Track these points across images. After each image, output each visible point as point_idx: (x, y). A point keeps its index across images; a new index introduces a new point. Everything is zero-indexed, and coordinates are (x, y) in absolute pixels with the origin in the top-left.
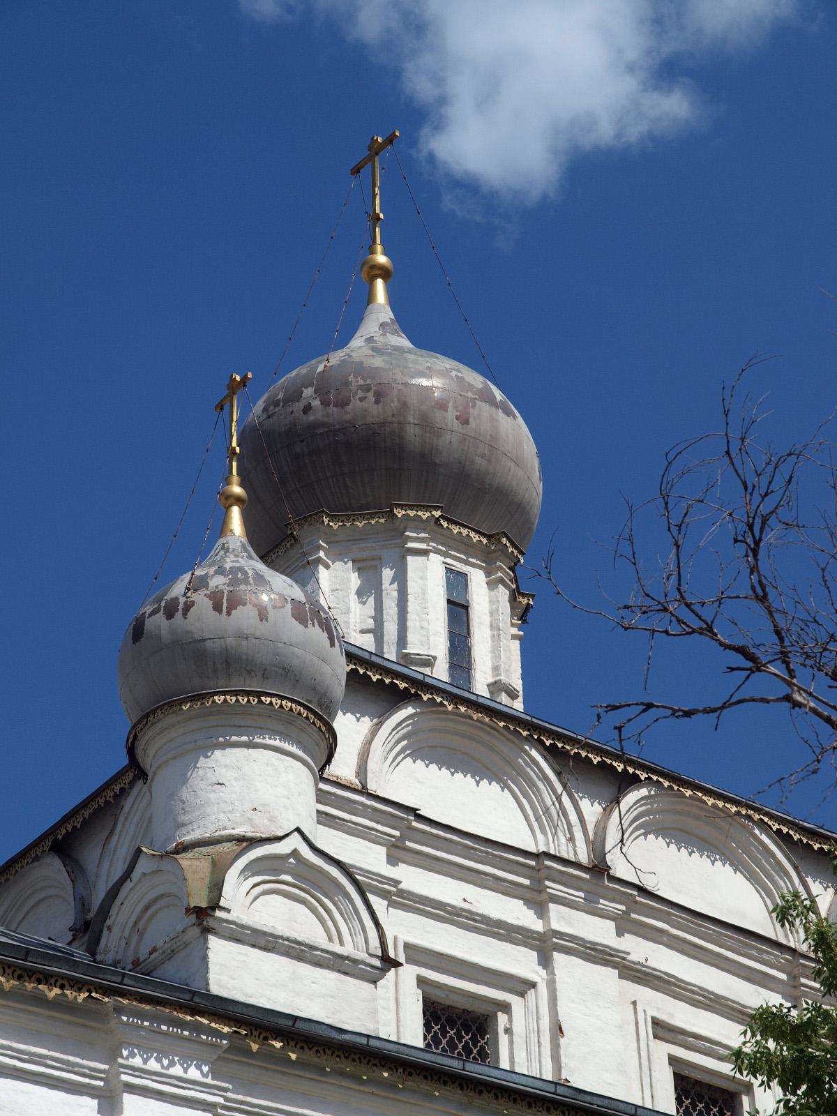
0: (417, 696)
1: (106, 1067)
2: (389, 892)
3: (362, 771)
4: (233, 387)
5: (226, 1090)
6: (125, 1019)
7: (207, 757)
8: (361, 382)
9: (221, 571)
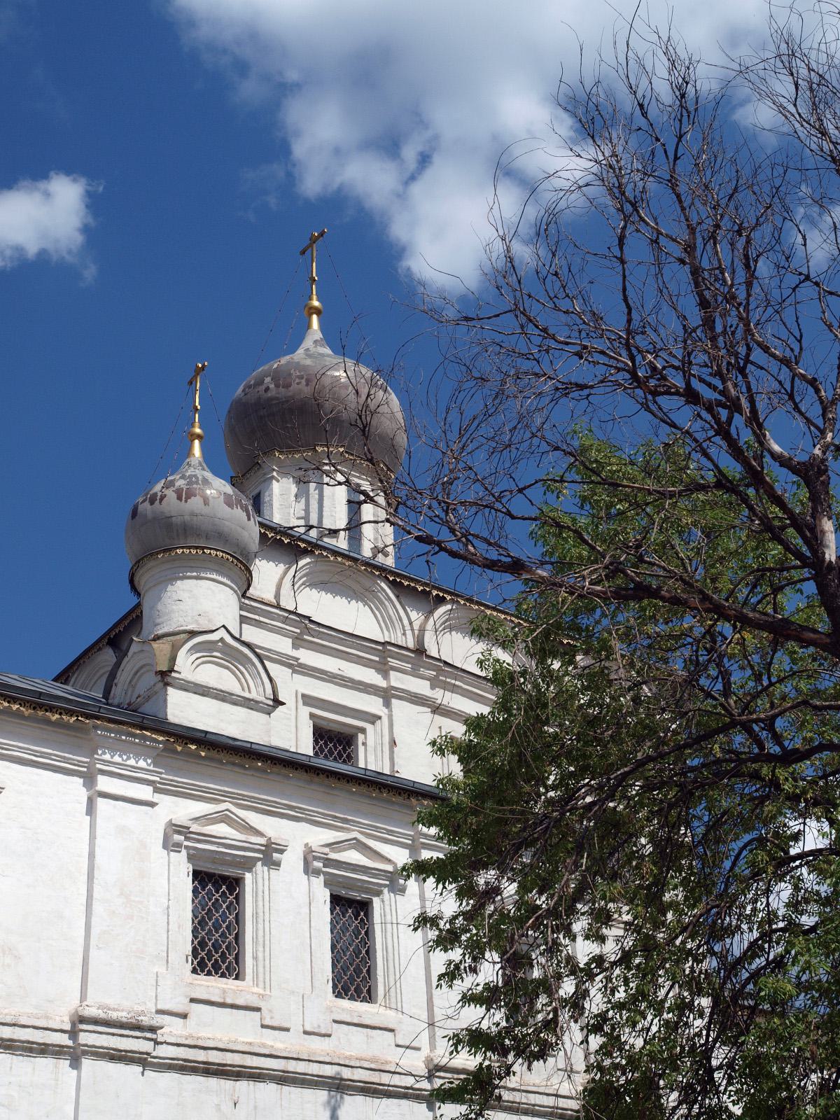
0: (312, 552)
1: (88, 760)
2: (293, 665)
3: (277, 596)
4: (198, 371)
5: (161, 773)
6: (99, 732)
7: (172, 585)
8: (298, 374)
9: (183, 477)
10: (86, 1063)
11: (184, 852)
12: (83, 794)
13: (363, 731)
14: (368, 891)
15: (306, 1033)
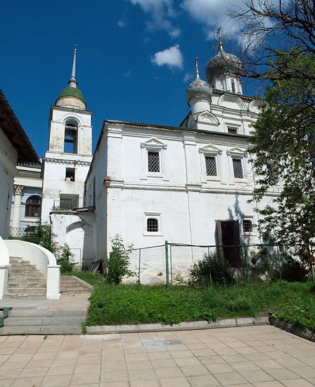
10: (189, 192)
11: (203, 153)
12: (182, 145)
13: (238, 128)
14: (240, 158)
15: (230, 185)
